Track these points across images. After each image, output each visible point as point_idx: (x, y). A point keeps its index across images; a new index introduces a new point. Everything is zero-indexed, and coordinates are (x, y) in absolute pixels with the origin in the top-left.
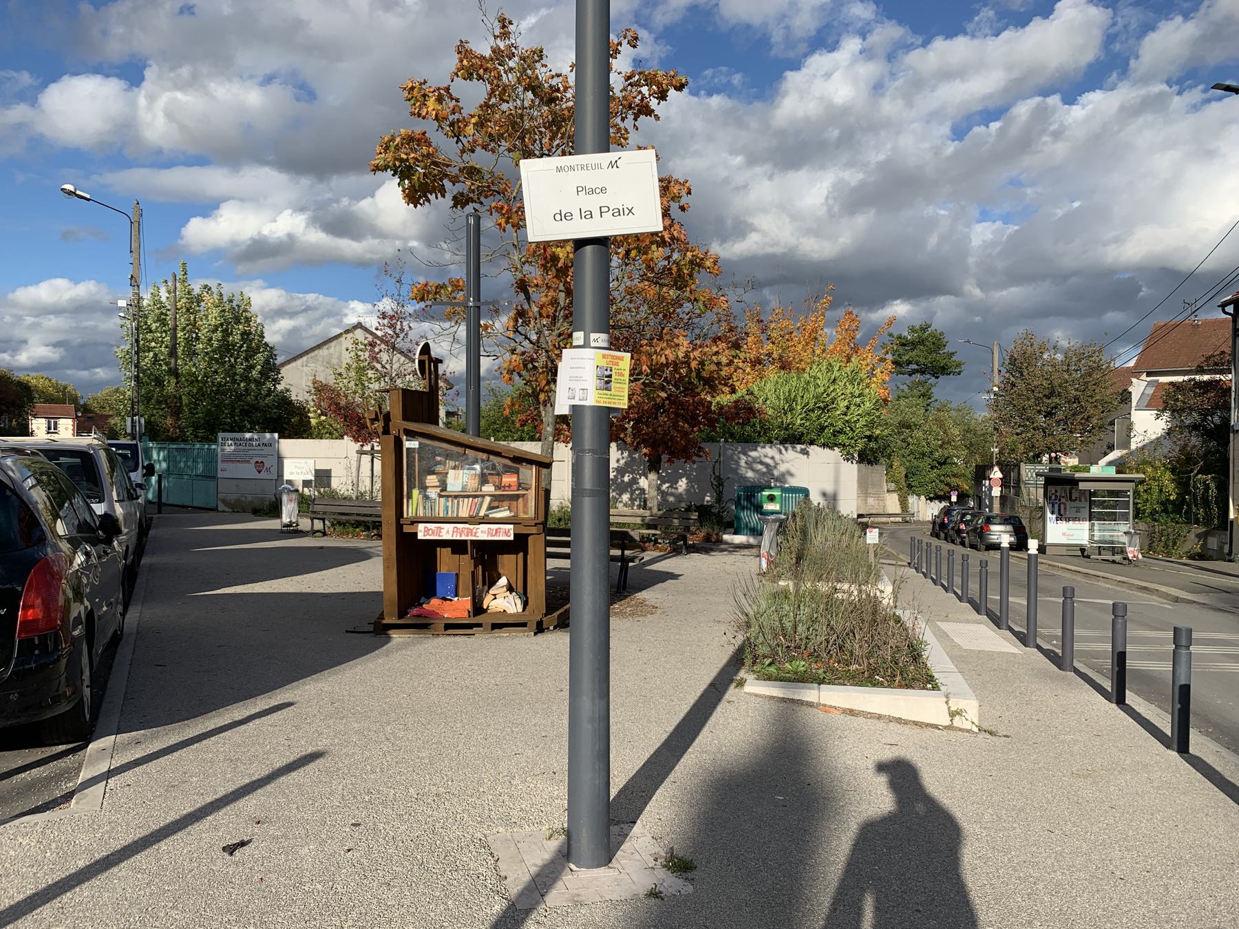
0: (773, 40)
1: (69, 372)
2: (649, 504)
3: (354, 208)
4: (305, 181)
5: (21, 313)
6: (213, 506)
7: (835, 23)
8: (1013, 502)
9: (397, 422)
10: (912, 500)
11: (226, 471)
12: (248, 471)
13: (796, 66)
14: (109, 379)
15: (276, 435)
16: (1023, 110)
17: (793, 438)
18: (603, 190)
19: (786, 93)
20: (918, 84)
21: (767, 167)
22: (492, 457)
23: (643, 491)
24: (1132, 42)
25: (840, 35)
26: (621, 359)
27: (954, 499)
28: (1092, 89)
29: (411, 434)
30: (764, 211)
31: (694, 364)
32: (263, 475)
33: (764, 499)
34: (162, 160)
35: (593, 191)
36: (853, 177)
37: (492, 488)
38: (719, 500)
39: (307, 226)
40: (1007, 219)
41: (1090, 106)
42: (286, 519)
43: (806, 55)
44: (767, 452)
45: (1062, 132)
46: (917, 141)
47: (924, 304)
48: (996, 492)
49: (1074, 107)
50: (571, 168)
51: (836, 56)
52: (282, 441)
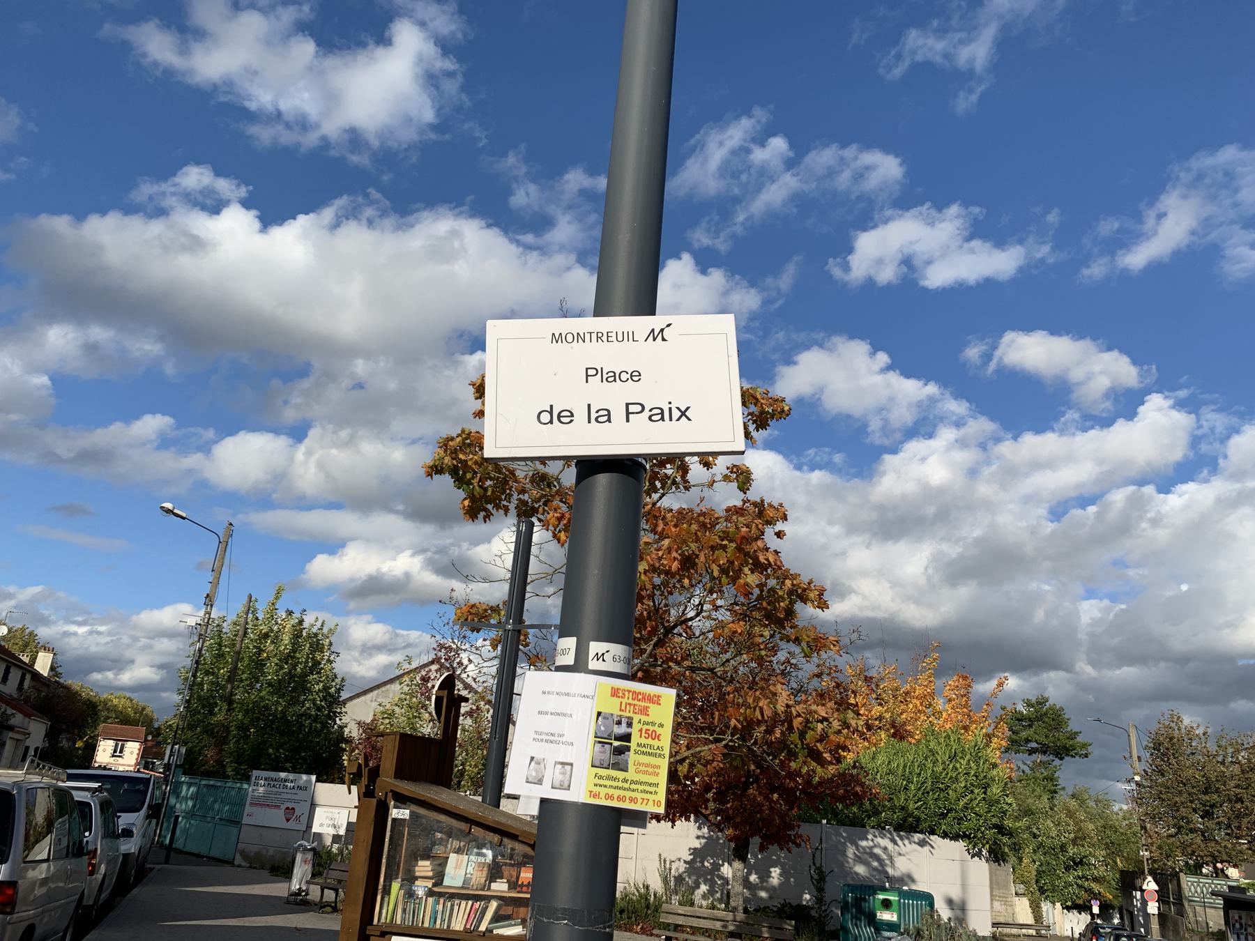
0: (869, 429)
1: (164, 695)
2: (733, 904)
3: (470, 552)
4: (429, 529)
5: (138, 634)
6: (228, 857)
7: (931, 417)
8: (1176, 924)
9: (387, 780)
10: (1045, 907)
11: (253, 816)
12: (275, 818)
13: (894, 450)
14: (168, 705)
15: (314, 778)
16: (1119, 497)
17: (908, 826)
18: (635, 376)
19: (884, 473)
20: (1011, 473)
21: (866, 537)
22: (506, 840)
23: (726, 881)
24: (1217, 445)
25: (935, 426)
26: (656, 700)
27: (1096, 910)
28: (1184, 481)
29: (402, 800)
30: (864, 574)
31: (797, 723)
32: (292, 825)
33: (878, 904)
34: (304, 504)
35: (614, 377)
36: (952, 550)
37: (505, 887)
38: (820, 900)
39: (422, 569)
40: (1114, 598)
41: (1186, 496)
42: (295, 886)
43: (902, 442)
44: (879, 842)
45: (1161, 520)
46: (1013, 518)
47: (1034, 679)
48: (1153, 908)
49: (1170, 496)
50: (579, 337)
51: (933, 443)
52: (319, 784)
